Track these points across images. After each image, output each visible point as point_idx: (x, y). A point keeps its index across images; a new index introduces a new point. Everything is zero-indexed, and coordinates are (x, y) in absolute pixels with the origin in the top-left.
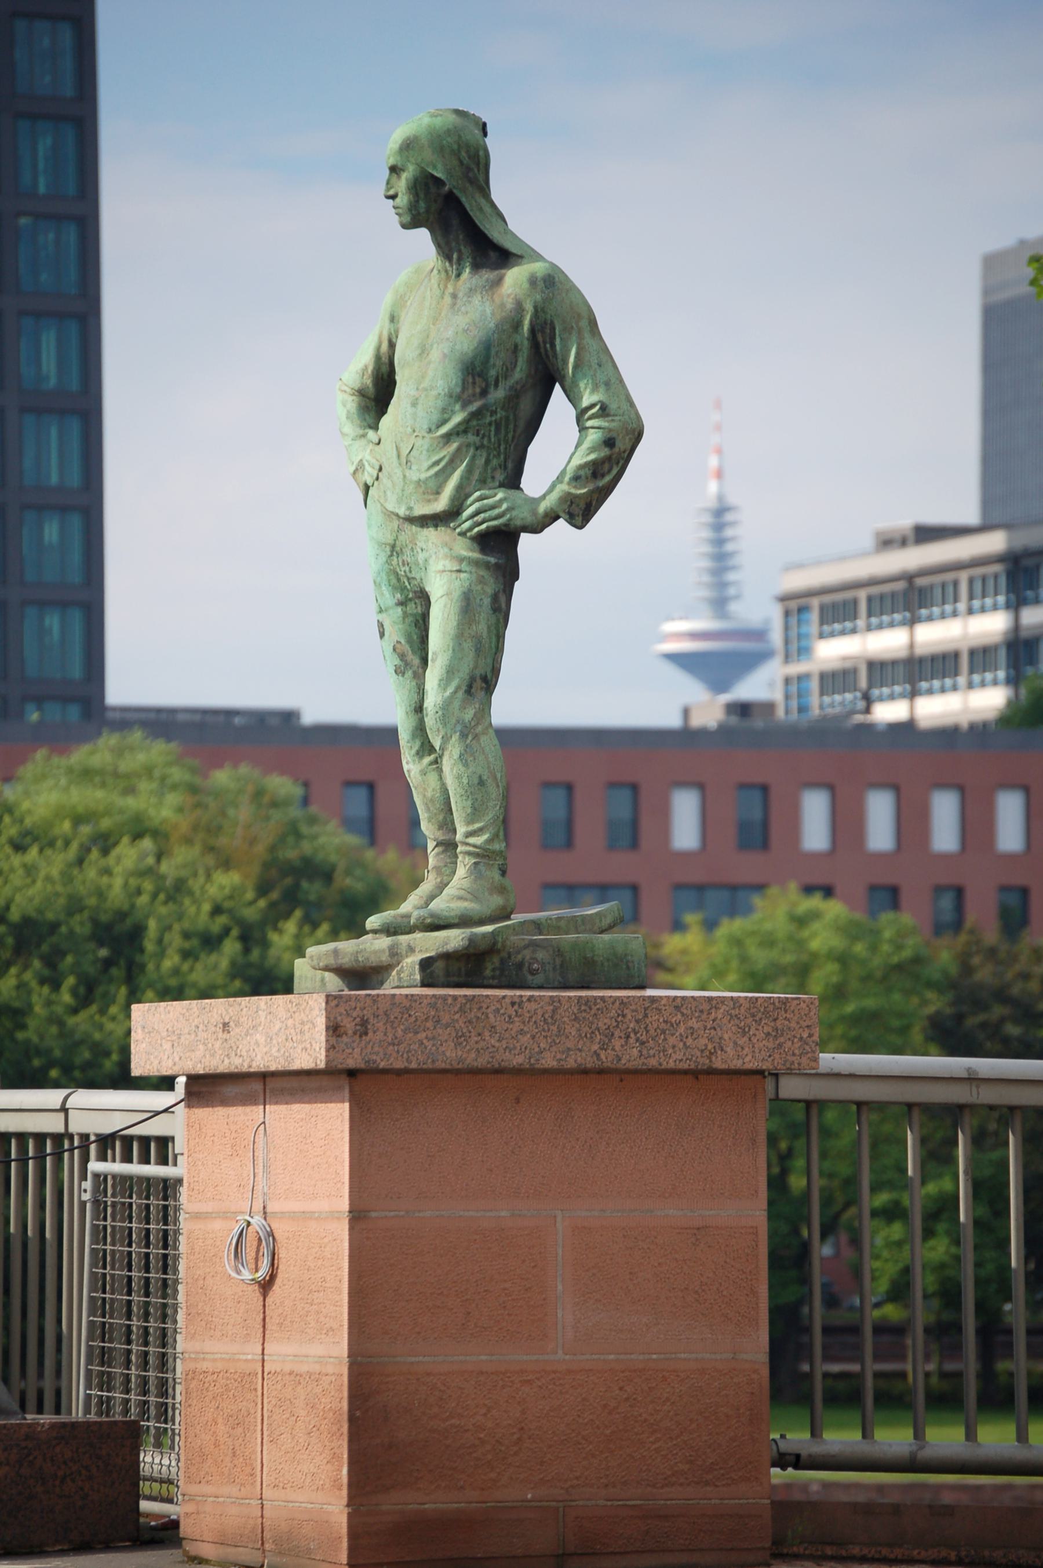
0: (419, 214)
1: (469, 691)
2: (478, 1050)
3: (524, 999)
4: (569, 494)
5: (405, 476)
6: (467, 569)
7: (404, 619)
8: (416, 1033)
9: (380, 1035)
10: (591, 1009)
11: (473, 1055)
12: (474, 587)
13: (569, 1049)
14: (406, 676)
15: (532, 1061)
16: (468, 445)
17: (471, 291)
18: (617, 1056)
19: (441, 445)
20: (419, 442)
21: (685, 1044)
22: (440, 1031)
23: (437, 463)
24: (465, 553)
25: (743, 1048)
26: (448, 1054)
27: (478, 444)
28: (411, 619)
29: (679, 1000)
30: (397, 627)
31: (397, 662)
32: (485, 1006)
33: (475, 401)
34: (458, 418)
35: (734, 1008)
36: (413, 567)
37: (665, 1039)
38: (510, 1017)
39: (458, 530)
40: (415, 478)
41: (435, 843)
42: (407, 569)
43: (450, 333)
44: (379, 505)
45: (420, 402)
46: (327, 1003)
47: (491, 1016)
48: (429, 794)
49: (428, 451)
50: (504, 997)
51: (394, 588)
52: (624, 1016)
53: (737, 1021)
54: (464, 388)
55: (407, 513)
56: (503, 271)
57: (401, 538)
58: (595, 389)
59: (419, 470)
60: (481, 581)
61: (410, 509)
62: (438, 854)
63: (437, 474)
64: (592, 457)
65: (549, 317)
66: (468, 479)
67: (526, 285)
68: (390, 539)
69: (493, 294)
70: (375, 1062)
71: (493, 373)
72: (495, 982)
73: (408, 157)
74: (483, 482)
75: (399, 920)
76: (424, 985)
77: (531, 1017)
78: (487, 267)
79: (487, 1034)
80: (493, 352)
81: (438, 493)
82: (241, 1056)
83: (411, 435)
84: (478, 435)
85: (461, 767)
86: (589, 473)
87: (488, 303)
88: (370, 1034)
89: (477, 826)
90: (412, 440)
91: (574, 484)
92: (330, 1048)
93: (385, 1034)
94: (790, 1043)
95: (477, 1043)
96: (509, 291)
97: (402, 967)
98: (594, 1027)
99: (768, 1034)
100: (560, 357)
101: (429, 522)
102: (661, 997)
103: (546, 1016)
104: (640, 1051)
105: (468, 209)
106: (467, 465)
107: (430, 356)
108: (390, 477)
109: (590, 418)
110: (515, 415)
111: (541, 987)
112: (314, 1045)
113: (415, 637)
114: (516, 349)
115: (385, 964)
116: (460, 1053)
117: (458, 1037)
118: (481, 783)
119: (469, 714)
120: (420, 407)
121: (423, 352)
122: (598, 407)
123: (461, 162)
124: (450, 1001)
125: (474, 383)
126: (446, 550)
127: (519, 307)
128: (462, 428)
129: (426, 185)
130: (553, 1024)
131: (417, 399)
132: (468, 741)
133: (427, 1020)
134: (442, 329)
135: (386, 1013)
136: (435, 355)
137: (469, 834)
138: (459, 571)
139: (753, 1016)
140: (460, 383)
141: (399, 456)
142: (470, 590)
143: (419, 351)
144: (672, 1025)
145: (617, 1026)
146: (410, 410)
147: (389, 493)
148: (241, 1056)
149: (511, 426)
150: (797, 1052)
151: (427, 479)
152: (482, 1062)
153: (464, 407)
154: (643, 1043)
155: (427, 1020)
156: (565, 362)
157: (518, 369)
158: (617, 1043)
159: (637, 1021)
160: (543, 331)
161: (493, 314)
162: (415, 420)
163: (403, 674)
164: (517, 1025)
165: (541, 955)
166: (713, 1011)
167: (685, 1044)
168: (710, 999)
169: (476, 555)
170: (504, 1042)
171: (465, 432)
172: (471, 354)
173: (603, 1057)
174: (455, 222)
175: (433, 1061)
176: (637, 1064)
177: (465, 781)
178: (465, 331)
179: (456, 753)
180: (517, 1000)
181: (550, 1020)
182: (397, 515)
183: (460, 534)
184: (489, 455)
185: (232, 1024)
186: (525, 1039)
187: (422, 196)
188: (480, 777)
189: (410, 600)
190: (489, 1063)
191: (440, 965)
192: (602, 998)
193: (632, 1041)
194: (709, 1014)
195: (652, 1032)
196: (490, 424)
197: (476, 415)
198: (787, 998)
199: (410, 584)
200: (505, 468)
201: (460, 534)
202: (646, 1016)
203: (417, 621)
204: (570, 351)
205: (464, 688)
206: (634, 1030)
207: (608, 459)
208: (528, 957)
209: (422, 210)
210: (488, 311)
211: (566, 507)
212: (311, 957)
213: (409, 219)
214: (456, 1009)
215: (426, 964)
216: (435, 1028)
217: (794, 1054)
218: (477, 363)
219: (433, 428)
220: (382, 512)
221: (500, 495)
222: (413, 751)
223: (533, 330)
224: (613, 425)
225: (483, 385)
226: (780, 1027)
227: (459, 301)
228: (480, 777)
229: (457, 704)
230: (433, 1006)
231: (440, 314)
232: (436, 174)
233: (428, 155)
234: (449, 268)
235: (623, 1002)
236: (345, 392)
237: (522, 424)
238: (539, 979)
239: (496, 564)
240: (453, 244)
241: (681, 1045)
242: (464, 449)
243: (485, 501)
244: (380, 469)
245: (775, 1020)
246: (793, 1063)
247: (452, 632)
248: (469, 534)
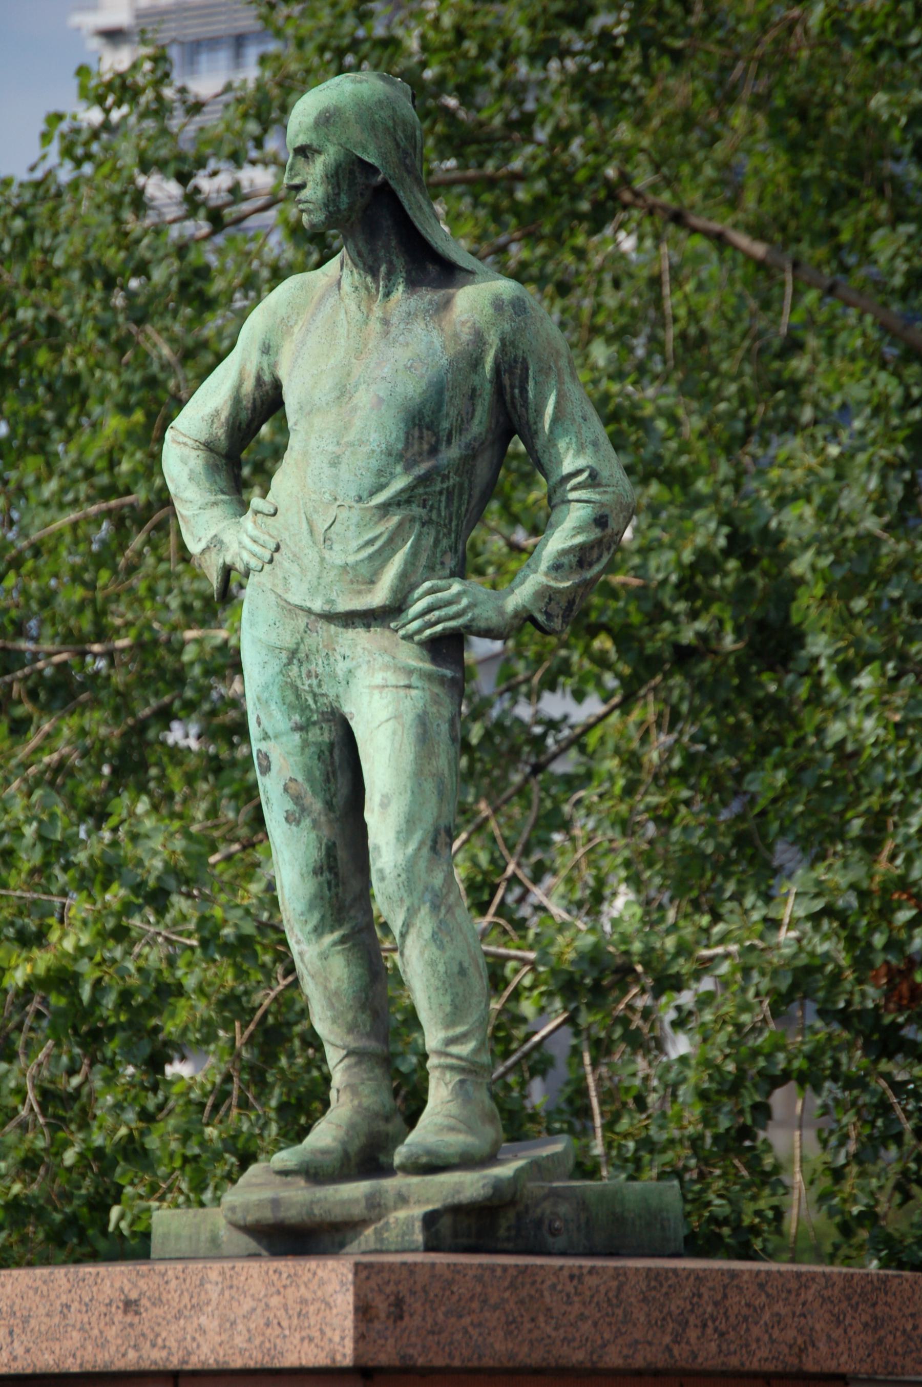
0: (339, 210)
1: (434, 849)
2: (531, 1342)
3: (585, 1271)
4: (549, 587)
5: (322, 559)
6: (419, 684)
7: (303, 749)
8: (460, 1317)
9: (417, 1320)
10: (661, 1285)
11: (526, 1349)
12: (429, 709)
13: (637, 1342)
14: (302, 825)
15: (595, 1358)
16: (413, 520)
17: (410, 316)
18: (693, 1352)
19: (375, 519)
20: (344, 514)
21: (770, 1336)
22: (487, 1314)
23: (371, 542)
24: (414, 663)
25: (837, 1345)
26: (497, 1346)
27: (425, 518)
28: (313, 749)
29: (763, 1276)
30: (291, 760)
31: (290, 806)
32: (539, 1280)
33: (422, 461)
34: (399, 483)
35: (826, 1288)
36: (326, 679)
37: (748, 1330)
38: (568, 1295)
39: (402, 632)
40: (339, 561)
41: (344, 1052)
42: (314, 682)
43: (387, 370)
44: (273, 597)
45: (344, 460)
46: (356, 1274)
47: (546, 1294)
48: (333, 985)
49: (358, 526)
50: (561, 1268)
51: (291, 707)
52: (700, 1296)
53: (830, 1306)
54: (408, 444)
55: (327, 608)
56: (451, 291)
57: (308, 641)
58: (580, 450)
59: (343, 551)
60: (436, 700)
61: (331, 602)
62: (349, 1067)
63: (371, 557)
64: (579, 539)
65: (520, 353)
66: (413, 564)
67: (489, 310)
68: (289, 641)
69: (440, 321)
70: (411, 1357)
71: (446, 425)
72: (510, 1246)
73: (327, 135)
74: (431, 570)
75: (319, 1157)
76: (429, 1248)
77: (592, 1297)
78: (428, 285)
79: (541, 1319)
80: (447, 398)
81: (372, 582)
82: (164, 1347)
83: (329, 504)
84: (424, 507)
85: (434, 949)
86: (574, 560)
87: (435, 333)
88: (407, 1318)
89: (460, 1030)
90: (333, 511)
91: (554, 574)
92: (360, 1338)
93: (424, 1319)
94: (891, 1338)
95: (530, 1331)
96: (464, 317)
97: (387, 1223)
98: (665, 1311)
99: (866, 1325)
100: (532, 406)
101: (357, 620)
102: (742, 1272)
103: (611, 1295)
104: (719, 1346)
105: (407, 207)
106: (412, 546)
107: (355, 401)
108: (296, 558)
109: (574, 489)
110: (470, 482)
111: (563, 1254)
112: (329, 1333)
113: (317, 773)
114: (473, 395)
115: (356, 1219)
116: (510, 1346)
117: (509, 1323)
118: (462, 972)
119: (438, 879)
120: (343, 467)
121: (342, 394)
122: (585, 475)
123: (398, 145)
124: (499, 1272)
125: (421, 438)
126: (387, 658)
127: (479, 338)
128: (405, 496)
129: (352, 172)
130: (618, 1306)
131: (338, 457)
132: (442, 916)
133: (472, 1298)
134: (372, 365)
135: (425, 1290)
136: (363, 398)
137: (451, 1041)
138: (409, 687)
139: (849, 1298)
140: (402, 436)
141: (311, 532)
142: (425, 713)
143: (337, 393)
144: (755, 1310)
145: (692, 1311)
146: (327, 471)
147: (293, 582)
148: (164, 1347)
149: (466, 497)
150: (900, 1350)
151: (357, 563)
152: (535, 1358)
153: (407, 469)
154: (722, 1335)
155: (472, 1298)
156: (540, 413)
157: (476, 421)
158: (693, 1334)
159: (716, 1304)
160: (511, 371)
161: (444, 347)
162: (336, 484)
163: (298, 823)
164: (577, 1308)
165: (564, 1209)
166: (803, 1291)
167: (770, 1336)
168: (799, 1275)
169: (428, 666)
170: (562, 1331)
171: (409, 502)
172: (418, 400)
173: (676, 1352)
174: (387, 222)
175: (480, 1358)
176: (714, 1363)
177: (441, 968)
178: (408, 368)
179: (427, 931)
180: (576, 1272)
181: (614, 1301)
182: (309, 611)
183: (404, 638)
184: (438, 533)
185: (144, 1302)
186: (586, 1327)
187: (345, 187)
188: (461, 964)
189: (314, 723)
190: (544, 1359)
191: (446, 1222)
192: (675, 1271)
193: (710, 1331)
194: (798, 1295)
195: (732, 1319)
196: (441, 493)
197: (424, 480)
198: (887, 1276)
199: (316, 702)
200: (456, 551)
201: (404, 638)
202: (725, 1296)
203: (322, 751)
204: (545, 399)
205: (429, 843)
206: (711, 1316)
207: (599, 543)
208: (548, 1212)
209: (343, 207)
210: (437, 343)
211: (542, 605)
212: (233, 1209)
213: (323, 217)
214: (506, 1284)
215: (430, 1220)
216: (482, 1310)
217: (896, 1354)
218: (427, 412)
219: (365, 495)
220: (278, 605)
221: (456, 587)
222: (310, 927)
223: (497, 370)
224: (605, 498)
225: (433, 440)
226: (880, 1315)
227: (393, 329)
228: (461, 964)
229: (422, 864)
230: (479, 1279)
231: (366, 345)
232: (366, 158)
233: (356, 133)
234: (372, 285)
235: (699, 1277)
236: (185, 444)
237: (477, 492)
238: (560, 1242)
239: (453, 679)
240: (382, 253)
241: (766, 1338)
242: (407, 525)
243: (439, 595)
244: (278, 549)
245: (874, 1305)
246: (895, 1365)
247: (409, 768)
248: (417, 638)
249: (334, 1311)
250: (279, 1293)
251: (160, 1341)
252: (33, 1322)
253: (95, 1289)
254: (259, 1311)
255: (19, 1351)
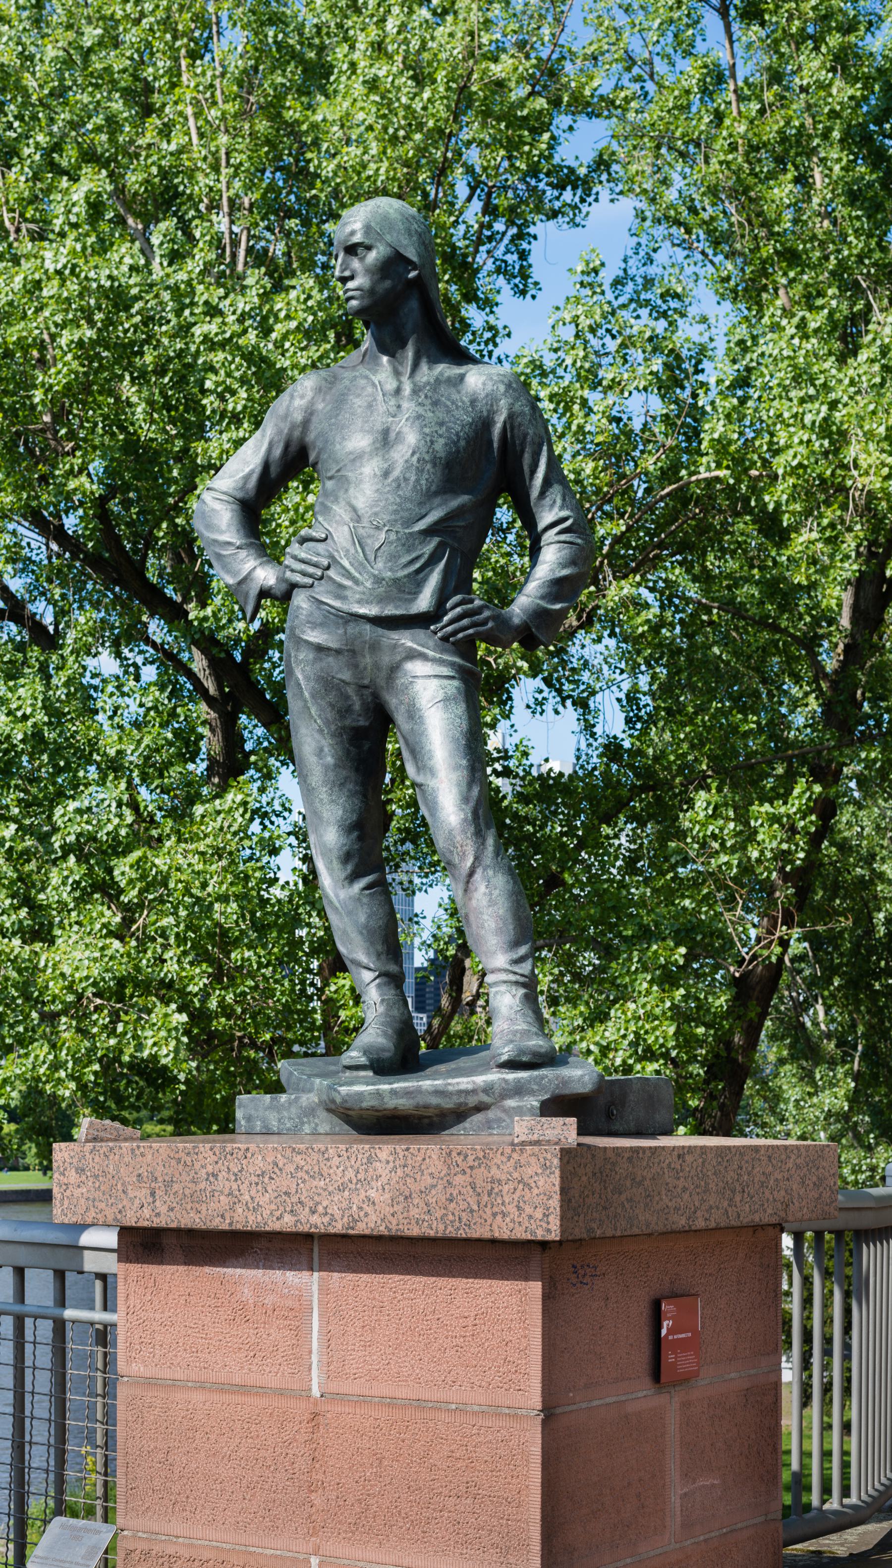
13: (711, 1207)
249: (535, 1191)
250: (464, 1172)
251: (320, 1209)
252: (176, 1187)
253: (244, 1162)
254: (440, 1187)
255: (163, 1209)
